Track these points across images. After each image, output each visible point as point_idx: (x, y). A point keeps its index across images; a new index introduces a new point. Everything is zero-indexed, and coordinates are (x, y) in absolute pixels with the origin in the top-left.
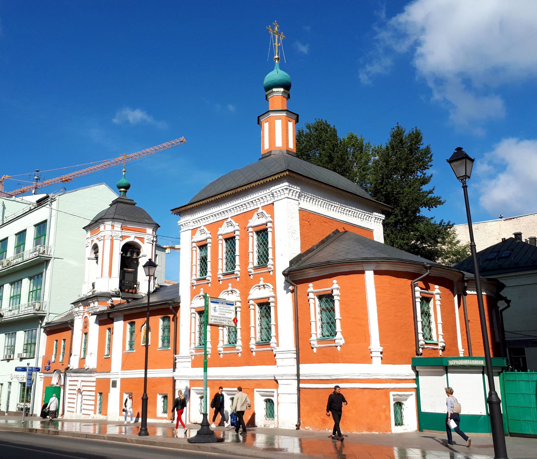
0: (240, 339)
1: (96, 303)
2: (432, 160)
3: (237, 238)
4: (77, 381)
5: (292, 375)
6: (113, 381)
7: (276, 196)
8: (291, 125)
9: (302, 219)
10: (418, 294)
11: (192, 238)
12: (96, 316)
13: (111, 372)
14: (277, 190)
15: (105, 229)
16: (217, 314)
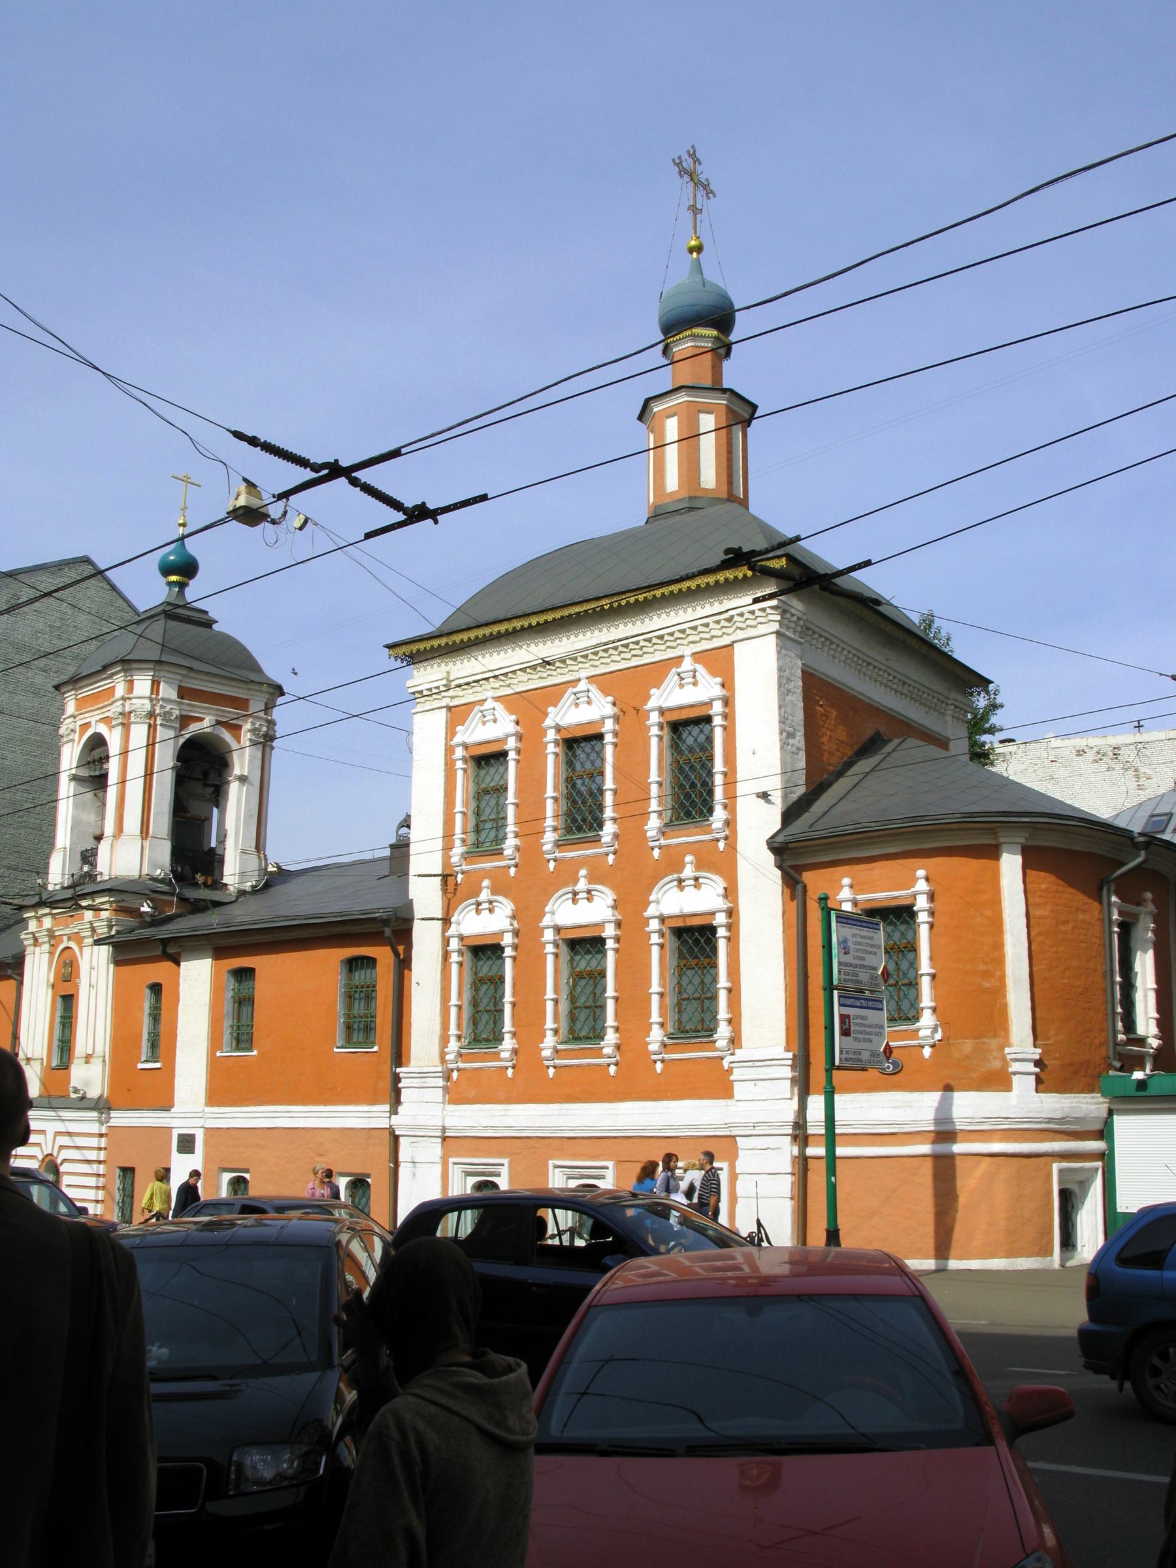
0: (612, 1027)
2: (929, 620)
5: (783, 1124)
6: (180, 1135)
13: (172, 1110)
15: (130, 689)
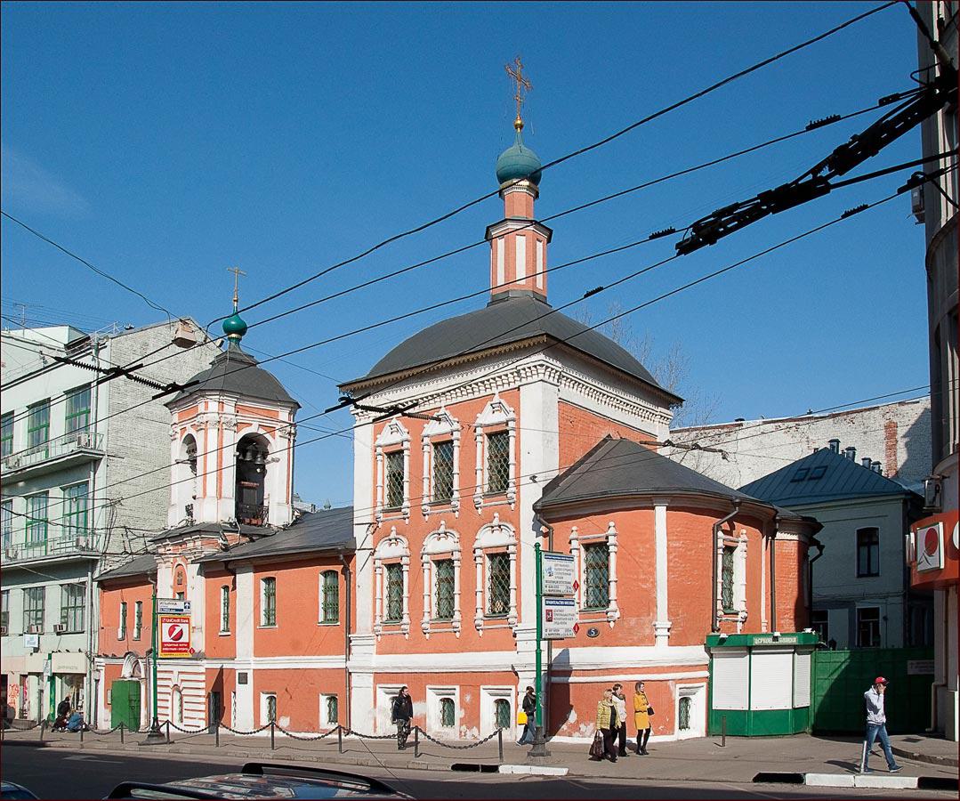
1: (198, 543)
3: (456, 443)
4: (172, 672)
6: (878, 608)
7: (524, 376)
8: (540, 245)
9: (562, 418)
10: (720, 543)
11: (376, 439)
12: (199, 565)
14: (526, 366)
15: (207, 407)
16: (552, 578)
